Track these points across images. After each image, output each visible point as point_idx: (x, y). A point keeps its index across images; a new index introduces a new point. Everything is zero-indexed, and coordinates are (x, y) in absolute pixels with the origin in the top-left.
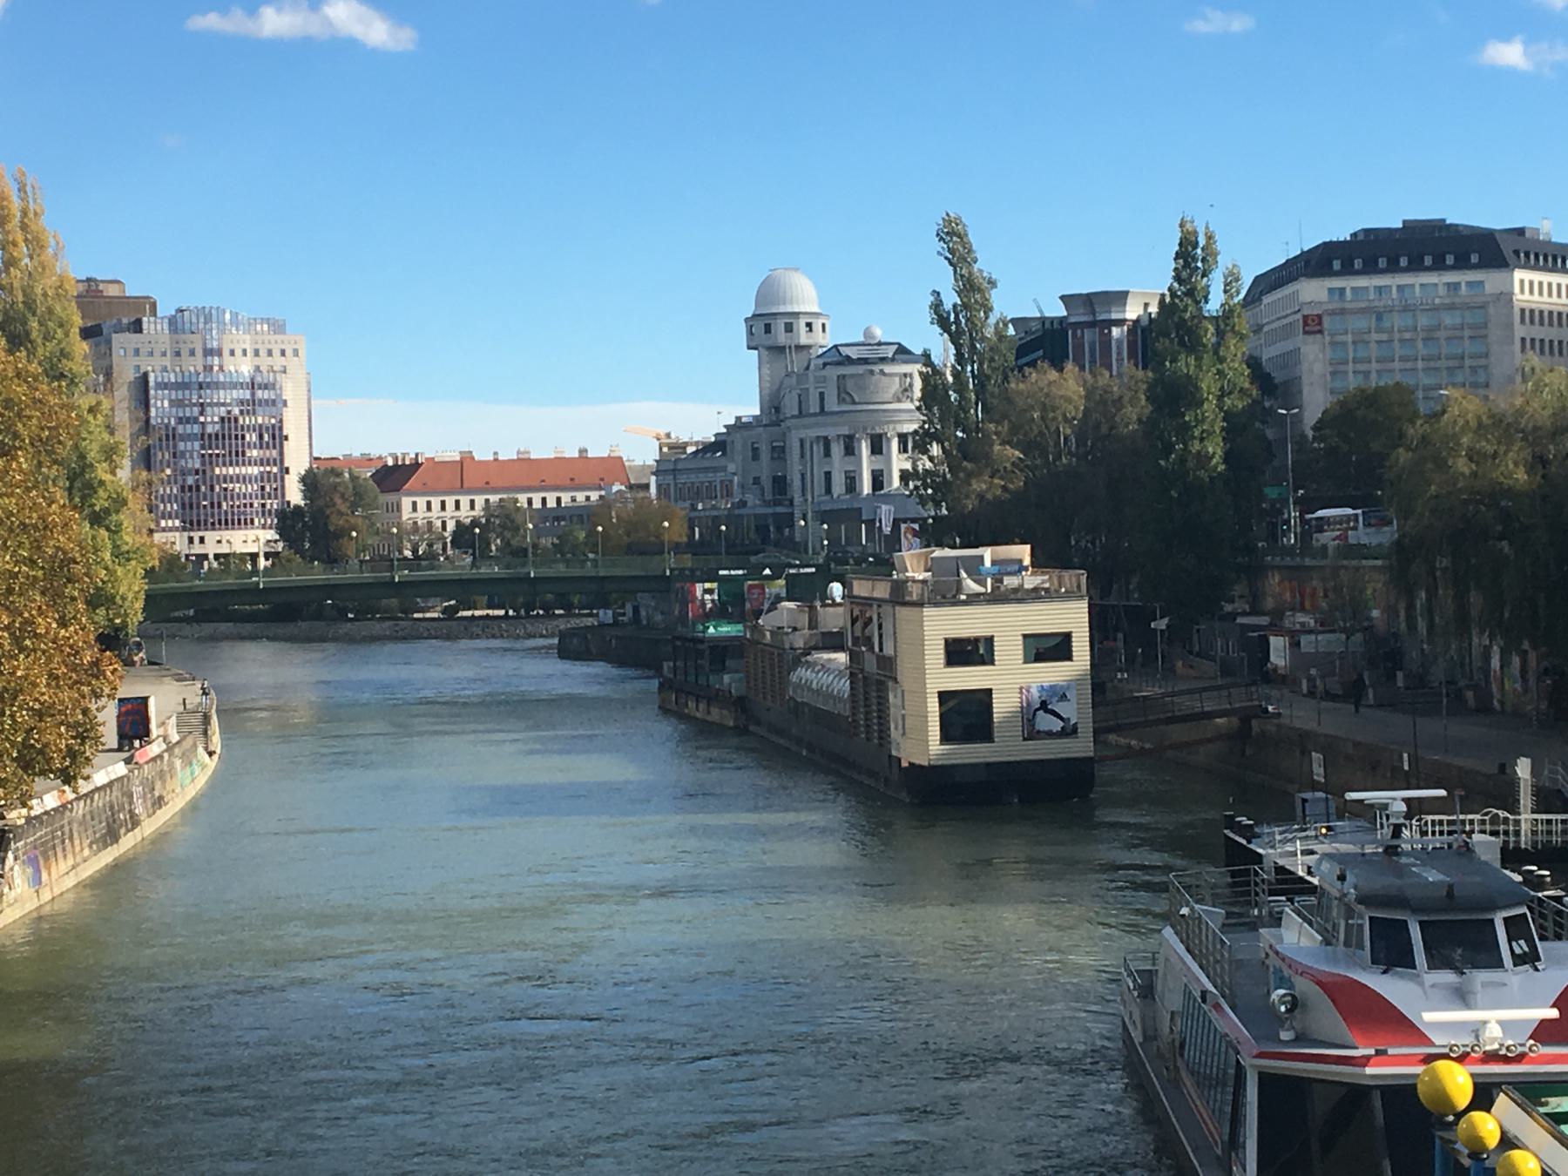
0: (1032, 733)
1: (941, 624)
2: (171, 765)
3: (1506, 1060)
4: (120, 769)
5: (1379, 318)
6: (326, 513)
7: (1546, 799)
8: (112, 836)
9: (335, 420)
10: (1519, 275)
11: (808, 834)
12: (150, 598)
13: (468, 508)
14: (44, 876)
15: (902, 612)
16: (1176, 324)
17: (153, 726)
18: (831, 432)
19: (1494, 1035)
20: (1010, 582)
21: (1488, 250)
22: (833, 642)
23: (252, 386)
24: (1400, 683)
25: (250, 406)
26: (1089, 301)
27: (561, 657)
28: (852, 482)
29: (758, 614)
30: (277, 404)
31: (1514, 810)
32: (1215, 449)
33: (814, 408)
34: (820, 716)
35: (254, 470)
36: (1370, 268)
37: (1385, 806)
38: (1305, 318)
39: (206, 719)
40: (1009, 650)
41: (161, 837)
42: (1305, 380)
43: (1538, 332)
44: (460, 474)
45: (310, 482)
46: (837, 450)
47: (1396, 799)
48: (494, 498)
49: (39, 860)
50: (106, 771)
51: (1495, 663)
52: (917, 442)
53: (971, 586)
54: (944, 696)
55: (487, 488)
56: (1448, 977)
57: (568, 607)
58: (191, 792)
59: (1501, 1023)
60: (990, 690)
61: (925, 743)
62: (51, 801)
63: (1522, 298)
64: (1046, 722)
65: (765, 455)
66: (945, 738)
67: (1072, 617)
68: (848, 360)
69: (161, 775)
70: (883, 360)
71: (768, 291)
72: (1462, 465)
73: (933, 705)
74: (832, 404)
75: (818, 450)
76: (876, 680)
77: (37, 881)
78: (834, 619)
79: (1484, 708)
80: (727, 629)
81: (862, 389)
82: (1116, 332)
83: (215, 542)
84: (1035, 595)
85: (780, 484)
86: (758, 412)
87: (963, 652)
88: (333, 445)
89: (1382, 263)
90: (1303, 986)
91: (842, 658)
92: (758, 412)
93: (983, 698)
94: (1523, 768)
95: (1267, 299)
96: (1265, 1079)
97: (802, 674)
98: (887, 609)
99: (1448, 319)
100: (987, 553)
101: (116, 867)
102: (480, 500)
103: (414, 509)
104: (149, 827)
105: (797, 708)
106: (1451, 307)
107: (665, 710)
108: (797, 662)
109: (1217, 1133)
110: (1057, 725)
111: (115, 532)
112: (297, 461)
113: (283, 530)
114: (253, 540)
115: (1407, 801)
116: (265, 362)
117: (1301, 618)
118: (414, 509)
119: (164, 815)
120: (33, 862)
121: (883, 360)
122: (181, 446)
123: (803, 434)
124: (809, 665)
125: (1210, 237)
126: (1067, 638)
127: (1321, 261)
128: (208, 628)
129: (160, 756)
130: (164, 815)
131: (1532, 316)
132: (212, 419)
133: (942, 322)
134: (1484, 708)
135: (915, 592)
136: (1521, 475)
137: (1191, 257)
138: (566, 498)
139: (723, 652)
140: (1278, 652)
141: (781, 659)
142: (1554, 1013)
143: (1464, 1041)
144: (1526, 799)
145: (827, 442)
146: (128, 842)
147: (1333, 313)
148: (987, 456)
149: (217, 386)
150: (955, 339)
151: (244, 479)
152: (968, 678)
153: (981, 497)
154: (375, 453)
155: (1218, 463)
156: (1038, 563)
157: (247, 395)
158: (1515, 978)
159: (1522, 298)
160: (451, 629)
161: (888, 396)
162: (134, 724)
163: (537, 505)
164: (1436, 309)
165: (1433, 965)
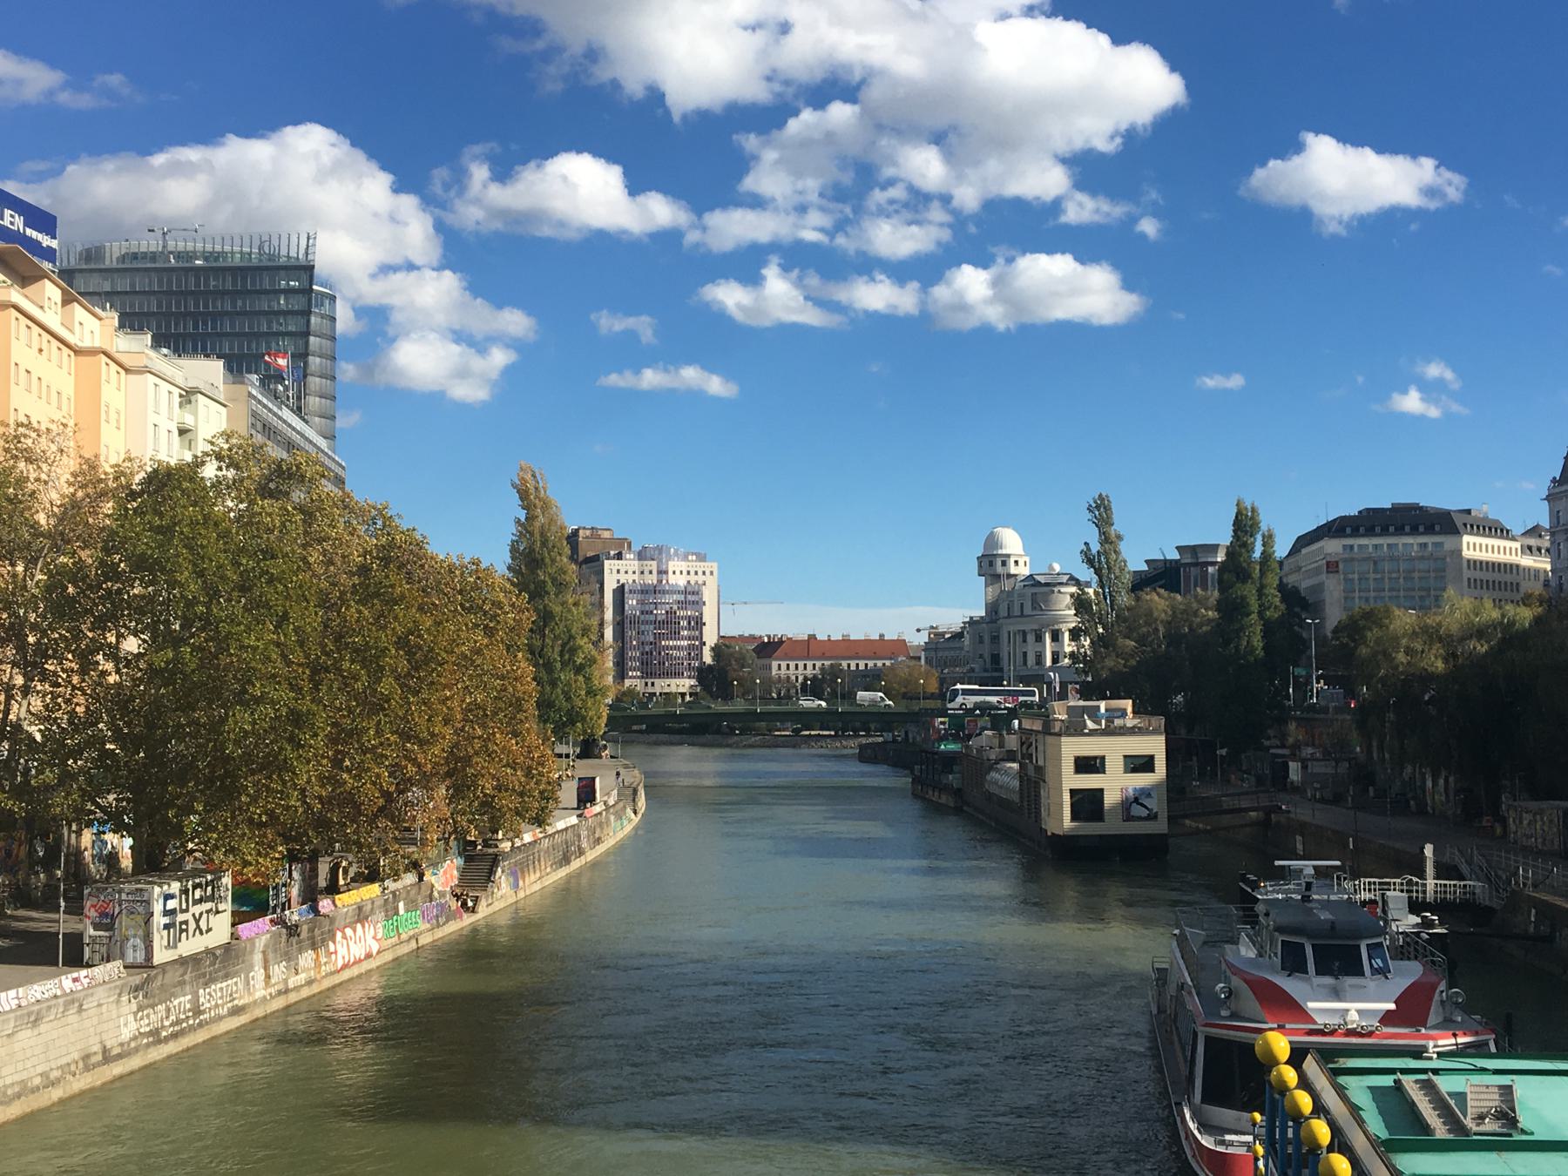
0: (1128, 818)
1: (1072, 748)
2: (608, 819)
3: (1361, 1035)
4: (574, 820)
5: (1375, 563)
6: (728, 669)
7: (1443, 871)
8: (566, 860)
9: (727, 618)
10: (1466, 539)
12: (610, 718)
15: (1050, 739)
16: (1236, 565)
17: (598, 795)
18: (1027, 628)
19: (1354, 1019)
20: (1118, 722)
21: (1444, 523)
22: (1011, 756)
23: (685, 592)
24: (1371, 793)
25: (683, 604)
26: (1194, 550)
27: (861, 761)
28: (1040, 658)
29: (969, 737)
30: (699, 604)
31: (1423, 877)
32: (1257, 642)
33: (1017, 612)
34: (1003, 803)
36: (1370, 532)
37: (1301, 871)
38: (1328, 563)
39: (635, 791)
40: (1115, 764)
41: (594, 865)
42: (1328, 601)
43: (1478, 575)
44: (808, 647)
45: (716, 650)
46: (1031, 638)
47: (1308, 866)
48: (827, 663)
49: (516, 875)
50: (563, 822)
51: (1429, 784)
52: (1075, 634)
53: (1090, 725)
54: (1072, 792)
55: (823, 657)
57: (868, 730)
58: (620, 835)
59: (1359, 1012)
63: (1468, 553)
65: (987, 639)
66: (1074, 818)
67: (1156, 746)
68: (1039, 584)
69: (601, 824)
70: (1061, 584)
71: (992, 541)
72: (1401, 657)
73: (1067, 797)
74: (1028, 611)
75: (1019, 638)
76: (1034, 781)
77: (516, 886)
78: (1012, 742)
79: (1422, 811)
80: (952, 747)
81: (1046, 602)
82: (1210, 569)
83: (662, 685)
84: (1133, 731)
85: (996, 659)
86: (983, 614)
87: (1087, 765)
88: (728, 631)
89: (1378, 529)
90: (1236, 982)
91: (1015, 766)
92: (983, 614)
93: (1098, 794)
94: (1429, 850)
95: (1304, 551)
96: (1208, 1039)
97: (994, 775)
98: (1040, 737)
99: (1422, 566)
100: (1103, 705)
101: (569, 877)
102: (818, 664)
103: (779, 668)
104: (591, 855)
105: (989, 797)
106: (1422, 558)
107: (915, 795)
108: (991, 768)
109: (1185, 1071)
110: (1145, 813)
112: (710, 637)
113: (700, 679)
114: (684, 685)
115: (1315, 867)
116: (693, 579)
117: (1310, 750)
118: (779, 668)
119: (601, 849)
120: (514, 874)
121: (1061, 584)
123: (1011, 628)
124: (998, 770)
125: (1253, 510)
126: (1152, 758)
128: (654, 737)
130: (601, 849)
132: (660, 612)
133: (1090, 561)
134: (1422, 811)
135: (1057, 727)
136: (1440, 665)
137: (1244, 524)
138: (888, 663)
139: (950, 760)
140: (1295, 772)
141: (980, 766)
142: (1392, 1006)
143: (1334, 1021)
144: (1430, 870)
145: (1024, 633)
146: (576, 864)
147: (1345, 560)
148: (1114, 646)
149: (664, 592)
150: (1098, 572)
152: (1089, 781)
154: (757, 633)
155: (1260, 652)
157: (681, 597)
158: (1370, 982)
159: (1468, 553)
160: (795, 741)
161: (1063, 606)
162: (586, 794)
163: (853, 668)
164: (1412, 559)
165: (1319, 973)
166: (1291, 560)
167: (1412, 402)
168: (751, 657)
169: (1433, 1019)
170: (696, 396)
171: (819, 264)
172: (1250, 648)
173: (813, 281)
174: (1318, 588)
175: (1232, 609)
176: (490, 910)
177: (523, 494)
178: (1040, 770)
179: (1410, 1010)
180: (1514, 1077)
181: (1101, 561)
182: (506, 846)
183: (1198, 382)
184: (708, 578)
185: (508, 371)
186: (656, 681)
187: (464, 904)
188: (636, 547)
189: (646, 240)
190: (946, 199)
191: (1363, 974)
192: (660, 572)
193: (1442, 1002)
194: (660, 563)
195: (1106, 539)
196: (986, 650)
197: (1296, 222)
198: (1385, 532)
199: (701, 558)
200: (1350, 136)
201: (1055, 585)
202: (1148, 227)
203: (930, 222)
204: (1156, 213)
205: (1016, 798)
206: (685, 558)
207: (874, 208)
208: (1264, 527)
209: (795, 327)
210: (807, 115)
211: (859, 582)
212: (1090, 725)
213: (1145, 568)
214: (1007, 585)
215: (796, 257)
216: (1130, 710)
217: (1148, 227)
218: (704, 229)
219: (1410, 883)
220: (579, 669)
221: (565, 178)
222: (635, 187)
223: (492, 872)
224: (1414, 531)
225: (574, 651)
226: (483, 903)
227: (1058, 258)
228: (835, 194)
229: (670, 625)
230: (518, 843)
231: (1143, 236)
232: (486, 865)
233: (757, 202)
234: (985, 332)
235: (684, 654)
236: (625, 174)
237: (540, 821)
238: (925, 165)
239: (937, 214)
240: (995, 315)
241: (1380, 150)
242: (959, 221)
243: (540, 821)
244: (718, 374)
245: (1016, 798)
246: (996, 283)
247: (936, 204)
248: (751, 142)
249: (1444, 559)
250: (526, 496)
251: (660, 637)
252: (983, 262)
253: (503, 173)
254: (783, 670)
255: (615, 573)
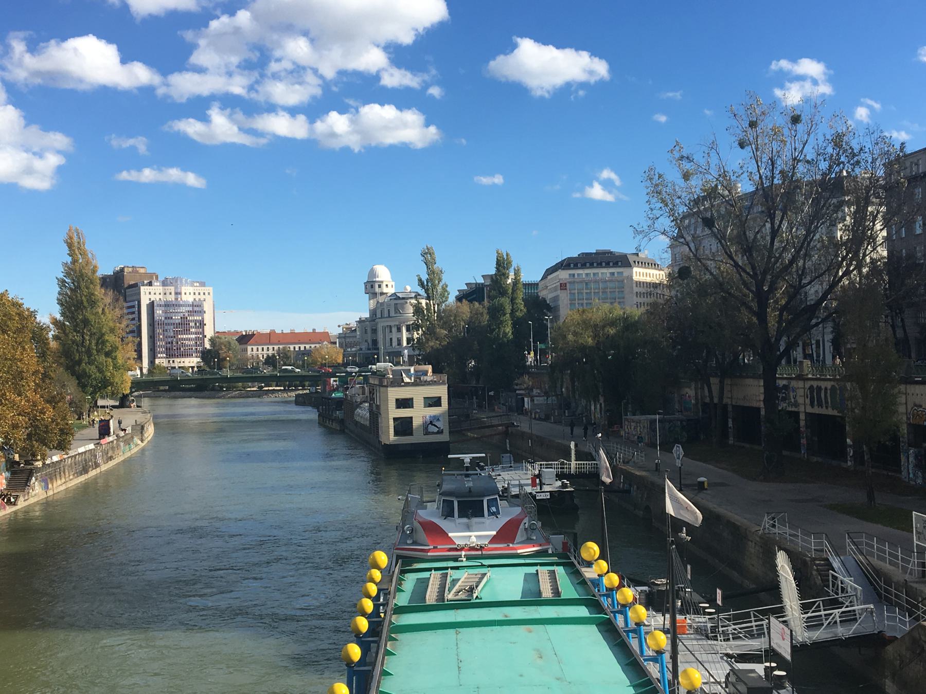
0: (427, 433)
1: (394, 394)
2: (118, 445)
3: (477, 550)
4: (92, 446)
5: (587, 284)
8: (85, 471)
9: (221, 320)
10: (635, 269)
11: (352, 469)
13: (270, 350)
14: (50, 486)
15: (382, 389)
18: (392, 324)
21: (622, 261)
30: (202, 312)
32: (509, 330)
33: (386, 315)
35: (194, 336)
36: (584, 266)
40: (419, 402)
44: (269, 338)
45: (212, 340)
46: (394, 330)
48: (281, 347)
51: (593, 408)
54: (394, 419)
55: (279, 343)
56: (465, 520)
57: (303, 386)
58: (128, 454)
60: (411, 418)
61: (390, 436)
62: (56, 458)
64: (432, 429)
66: (396, 434)
67: (442, 391)
69: (113, 448)
71: (372, 273)
73: (391, 422)
74: (392, 314)
75: (387, 330)
76: (376, 414)
81: (403, 308)
83: (179, 362)
85: (375, 342)
86: (368, 316)
87: (405, 403)
92: (368, 316)
95: (549, 277)
99: (609, 284)
102: (276, 347)
104: (104, 468)
105: (357, 423)
106: (611, 281)
110: (436, 430)
111: (115, 359)
112: (209, 332)
113: (203, 358)
116: (197, 297)
119: (111, 464)
122: (166, 327)
125: (507, 255)
126: (440, 398)
127: (566, 264)
128: (173, 394)
129: (112, 442)
130: (111, 464)
131: (639, 284)
137: (502, 264)
138: (308, 346)
139: (339, 403)
146: (92, 473)
147: (570, 283)
149: (180, 306)
150: (427, 291)
151: (189, 339)
152: (404, 413)
153: (432, 347)
154: (239, 330)
156: (434, 371)
158: (487, 520)
160: (260, 393)
164: (606, 281)
165: (459, 517)
166: (543, 282)
167: (597, 192)
168: (235, 344)
169: (519, 538)
170: (180, 187)
171: (245, 107)
172: (505, 334)
173: (240, 116)
174: (556, 299)
175: (496, 312)
176: (27, 503)
177: (70, 246)
178: (378, 407)
179: (506, 534)
180: (538, 568)
181: (430, 285)
182: (39, 464)
183: (475, 179)
184: (207, 296)
185: (59, 170)
186: (176, 360)
187: (9, 500)
188: (161, 278)
189: (135, 91)
190: (315, 71)
191: (483, 516)
192: (176, 293)
193: (526, 529)
194: (176, 288)
195: (431, 272)
196: (369, 337)
197: (517, 91)
198: (592, 266)
199: (203, 284)
200: (543, 39)
201: (408, 298)
202: (435, 91)
203: (308, 83)
204: (438, 83)
205: (367, 423)
206: (192, 285)
207: (269, 74)
208: (514, 265)
209: (233, 145)
210: (225, 19)
211: (293, 296)
212: (407, 380)
213: (466, 288)
214: (381, 299)
215: (229, 102)
216: (430, 370)
217: (435, 91)
218: (168, 85)
219: (562, 463)
220: (108, 354)
221: (75, 50)
222: (126, 58)
223: (28, 480)
224: (608, 265)
225: (104, 343)
226: (21, 499)
227: (387, 107)
228: (246, 66)
229: (184, 325)
230: (48, 462)
231: (432, 97)
232: (24, 476)
233: (200, 70)
234: (346, 150)
235: (192, 343)
236: (119, 50)
237: (62, 446)
238: (298, 48)
239: (310, 78)
240: (354, 142)
241: (559, 46)
242: (326, 85)
243: (62, 446)
244: (193, 172)
245: (367, 423)
246: (352, 122)
247: (309, 72)
248: (189, 35)
249: (623, 281)
250: (73, 246)
251: (177, 333)
252: (342, 111)
253: (33, 47)
254: (255, 352)
255: (147, 295)
